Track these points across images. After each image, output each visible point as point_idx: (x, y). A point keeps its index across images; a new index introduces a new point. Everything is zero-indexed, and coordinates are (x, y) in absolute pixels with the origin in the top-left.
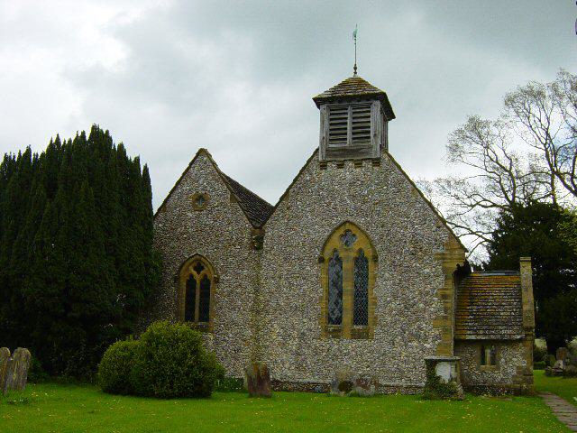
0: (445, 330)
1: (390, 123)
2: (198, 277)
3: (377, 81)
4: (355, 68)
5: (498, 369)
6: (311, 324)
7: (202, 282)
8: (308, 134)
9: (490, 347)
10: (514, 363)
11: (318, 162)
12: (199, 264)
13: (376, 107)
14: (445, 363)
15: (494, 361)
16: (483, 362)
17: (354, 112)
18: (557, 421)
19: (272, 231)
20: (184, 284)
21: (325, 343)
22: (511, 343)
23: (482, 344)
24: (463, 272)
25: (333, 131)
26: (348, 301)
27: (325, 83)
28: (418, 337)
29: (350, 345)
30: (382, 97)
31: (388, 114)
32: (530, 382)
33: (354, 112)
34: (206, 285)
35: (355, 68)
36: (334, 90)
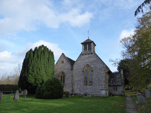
0: (106, 84)
1: (95, 47)
2: (62, 75)
3: (92, 39)
4: (88, 37)
5: (117, 91)
6: (82, 83)
7: (63, 76)
8: (80, 49)
9: (116, 87)
10: (120, 90)
11: (82, 54)
12: (63, 73)
13: (92, 43)
14: (104, 90)
15: (116, 89)
16: (114, 90)
17: (88, 45)
18: (141, 93)
19: (75, 66)
20: (60, 77)
21: (84, 87)
22: (120, 86)
23: (114, 86)
24: (109, 72)
25: (85, 49)
26: (39, 57)
27: (84, 40)
28: (101, 85)
29: (88, 87)
30: (93, 42)
31: (95, 45)
32: (124, 93)
33: (88, 45)
34: (64, 77)
35: (88, 37)
36: (85, 42)
